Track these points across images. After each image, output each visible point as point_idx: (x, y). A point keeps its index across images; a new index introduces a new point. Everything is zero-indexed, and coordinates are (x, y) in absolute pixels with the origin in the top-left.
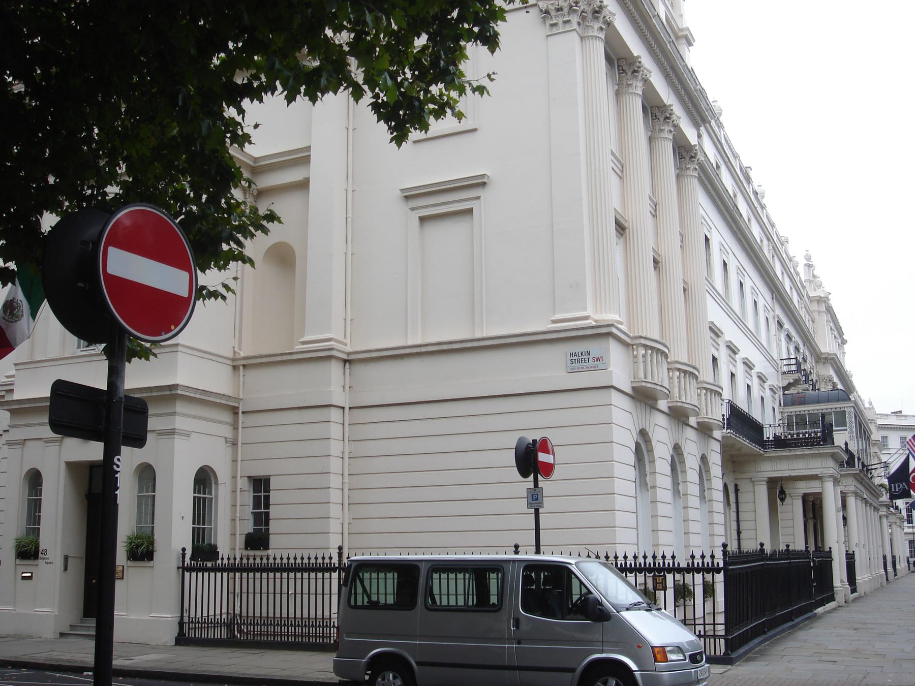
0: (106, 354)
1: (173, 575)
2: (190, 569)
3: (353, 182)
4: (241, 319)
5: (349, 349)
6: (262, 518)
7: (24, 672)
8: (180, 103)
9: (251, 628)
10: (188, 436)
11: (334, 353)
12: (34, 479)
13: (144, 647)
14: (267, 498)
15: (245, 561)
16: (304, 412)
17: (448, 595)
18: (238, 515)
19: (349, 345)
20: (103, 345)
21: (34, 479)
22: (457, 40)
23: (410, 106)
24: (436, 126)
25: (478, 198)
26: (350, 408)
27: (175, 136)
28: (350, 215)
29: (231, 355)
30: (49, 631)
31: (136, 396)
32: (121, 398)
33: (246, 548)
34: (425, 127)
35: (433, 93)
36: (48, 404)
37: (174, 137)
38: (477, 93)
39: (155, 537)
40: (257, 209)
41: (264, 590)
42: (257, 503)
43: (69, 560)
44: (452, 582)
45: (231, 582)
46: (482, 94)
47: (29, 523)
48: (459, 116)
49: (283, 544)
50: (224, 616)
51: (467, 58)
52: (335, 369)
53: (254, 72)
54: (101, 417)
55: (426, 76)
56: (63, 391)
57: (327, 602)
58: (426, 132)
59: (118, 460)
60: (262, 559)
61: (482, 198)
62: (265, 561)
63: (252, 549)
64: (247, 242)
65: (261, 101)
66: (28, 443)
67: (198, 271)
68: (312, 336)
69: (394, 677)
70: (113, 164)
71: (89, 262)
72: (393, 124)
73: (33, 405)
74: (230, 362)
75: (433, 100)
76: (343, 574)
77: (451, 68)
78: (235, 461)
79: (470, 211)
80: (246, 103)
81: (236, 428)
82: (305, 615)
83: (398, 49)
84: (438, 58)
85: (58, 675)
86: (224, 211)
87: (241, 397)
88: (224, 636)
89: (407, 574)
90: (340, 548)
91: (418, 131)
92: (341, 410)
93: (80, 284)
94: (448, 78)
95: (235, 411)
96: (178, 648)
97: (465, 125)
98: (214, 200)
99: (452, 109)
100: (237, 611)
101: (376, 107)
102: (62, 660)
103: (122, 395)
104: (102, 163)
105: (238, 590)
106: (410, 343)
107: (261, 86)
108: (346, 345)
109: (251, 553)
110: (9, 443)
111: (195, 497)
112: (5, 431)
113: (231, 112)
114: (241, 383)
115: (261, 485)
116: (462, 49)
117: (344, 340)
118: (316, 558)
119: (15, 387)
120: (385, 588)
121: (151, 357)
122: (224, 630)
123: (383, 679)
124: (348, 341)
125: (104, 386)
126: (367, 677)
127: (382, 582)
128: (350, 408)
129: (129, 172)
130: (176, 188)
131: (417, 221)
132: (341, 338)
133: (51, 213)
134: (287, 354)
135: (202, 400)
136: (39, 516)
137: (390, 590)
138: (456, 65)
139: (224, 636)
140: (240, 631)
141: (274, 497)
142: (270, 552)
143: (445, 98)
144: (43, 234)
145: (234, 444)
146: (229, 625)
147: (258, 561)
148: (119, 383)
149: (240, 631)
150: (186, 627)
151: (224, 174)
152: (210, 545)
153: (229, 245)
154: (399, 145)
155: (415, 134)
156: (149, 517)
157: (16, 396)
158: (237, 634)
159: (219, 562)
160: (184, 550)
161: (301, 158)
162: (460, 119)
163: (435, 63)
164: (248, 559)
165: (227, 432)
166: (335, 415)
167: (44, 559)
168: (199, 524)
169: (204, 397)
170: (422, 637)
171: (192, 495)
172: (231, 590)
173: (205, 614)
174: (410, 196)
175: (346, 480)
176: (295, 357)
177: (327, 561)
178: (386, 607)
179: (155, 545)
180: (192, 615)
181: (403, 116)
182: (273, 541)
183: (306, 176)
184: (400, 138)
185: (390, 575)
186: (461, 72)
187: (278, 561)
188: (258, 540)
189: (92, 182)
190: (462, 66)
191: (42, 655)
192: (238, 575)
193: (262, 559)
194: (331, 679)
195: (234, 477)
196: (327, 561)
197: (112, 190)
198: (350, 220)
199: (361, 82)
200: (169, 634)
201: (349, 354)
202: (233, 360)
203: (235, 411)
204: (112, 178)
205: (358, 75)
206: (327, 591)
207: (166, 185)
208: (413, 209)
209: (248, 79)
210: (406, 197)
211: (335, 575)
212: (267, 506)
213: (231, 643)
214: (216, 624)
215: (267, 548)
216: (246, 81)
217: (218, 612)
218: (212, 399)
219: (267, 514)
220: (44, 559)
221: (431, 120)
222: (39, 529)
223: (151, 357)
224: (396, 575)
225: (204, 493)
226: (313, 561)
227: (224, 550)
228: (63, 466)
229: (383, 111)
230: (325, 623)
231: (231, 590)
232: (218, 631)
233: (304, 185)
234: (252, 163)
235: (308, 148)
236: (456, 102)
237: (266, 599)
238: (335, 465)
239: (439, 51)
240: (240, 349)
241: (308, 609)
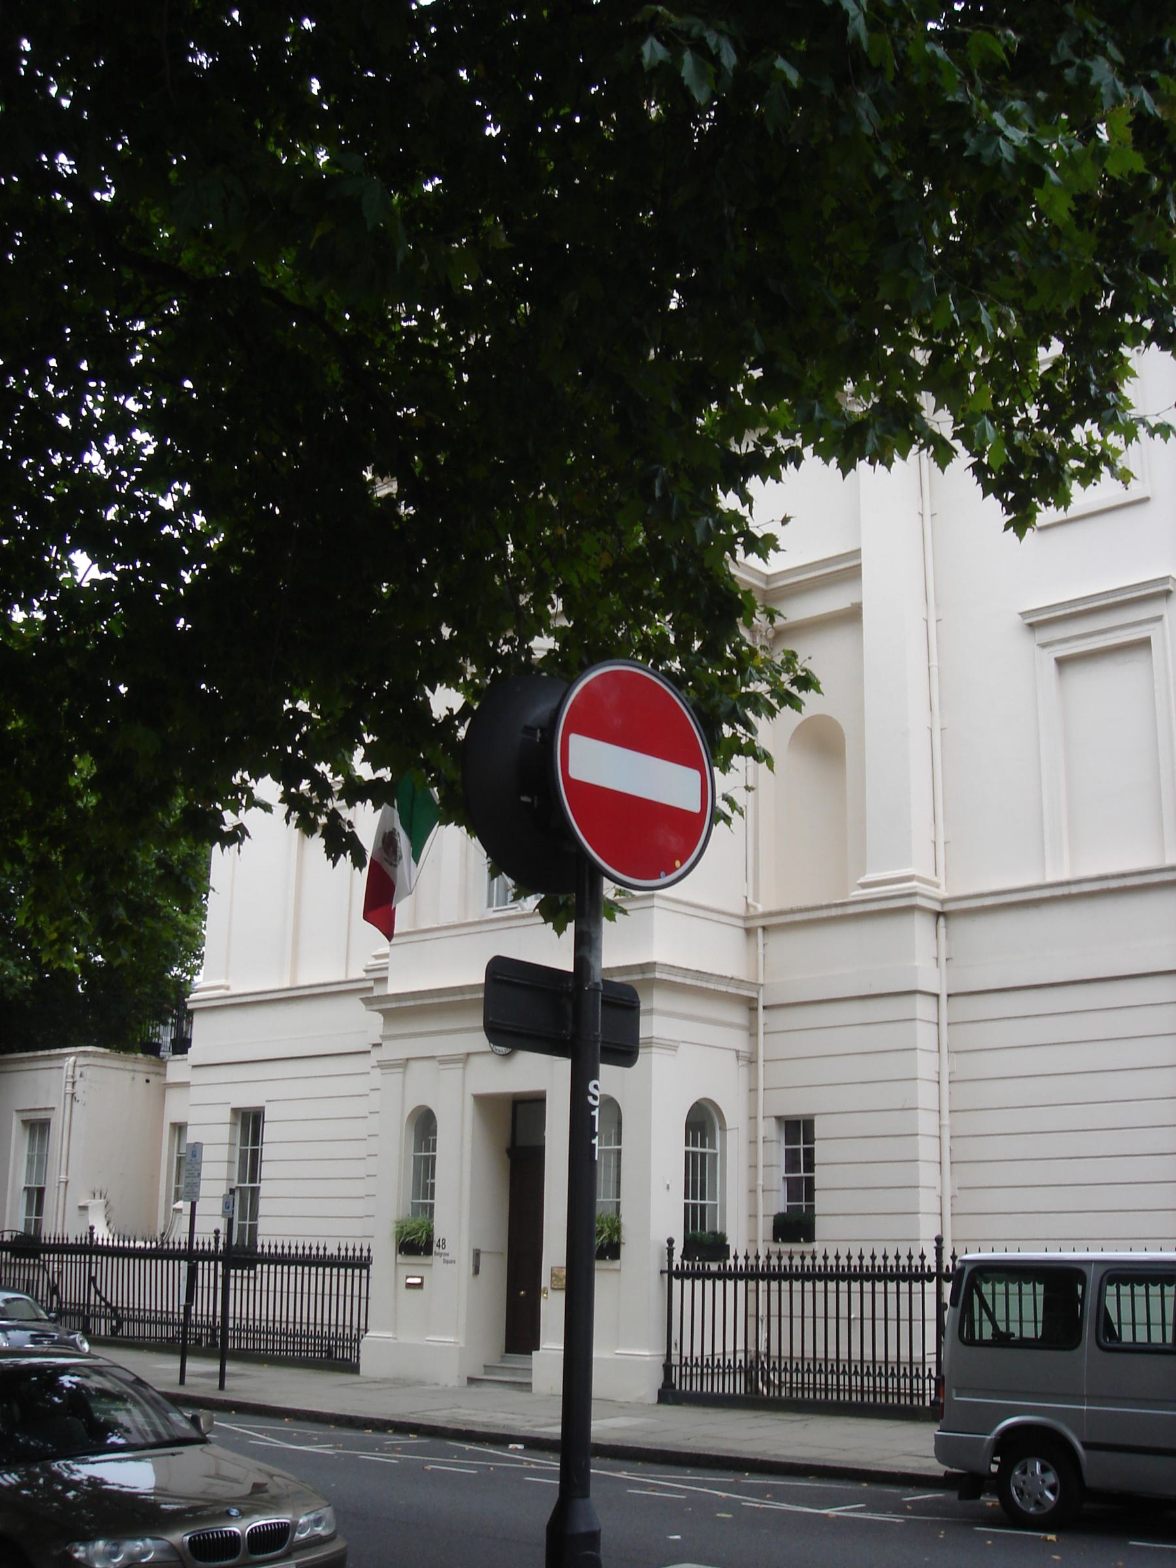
0: (542, 913)
1: (654, 1284)
2: (682, 1275)
3: (937, 605)
4: (756, 849)
5: (943, 893)
6: (801, 1188)
7: (413, 1439)
8: (658, 493)
9: (786, 1377)
10: (674, 1048)
11: (919, 901)
12: (424, 1124)
13: (624, 1408)
14: (809, 1153)
15: (774, 1261)
16: (871, 1004)
17: (1134, 1324)
18: (760, 1182)
19: (943, 887)
20: (543, 896)
21: (424, 1124)
22: (1114, 344)
23: (1040, 464)
24: (1082, 497)
25: (1159, 619)
26: (949, 996)
27: (641, 547)
28: (934, 662)
29: (741, 911)
30: (450, 1374)
31: (617, 979)
32: (597, 984)
33: (775, 1240)
34: (1063, 500)
35: (1077, 439)
36: (482, 995)
37: (639, 550)
38: (1157, 436)
39: (623, 1220)
40: (771, 661)
41: (892, 1313)
42: (792, 1162)
43: (482, 1256)
44: (1140, 1302)
45: (752, 1296)
46: (1166, 437)
47: (416, 1195)
48: (1125, 477)
49: (837, 1235)
50: (740, 1356)
51: (1134, 375)
52: (921, 927)
53: (763, 431)
54: (570, 1014)
55: (1060, 417)
56: (504, 973)
57: (916, 1332)
58: (1065, 510)
59: (596, 1087)
60: (803, 1258)
61: (1166, 619)
62: (808, 1261)
63: (785, 1240)
64: (761, 723)
65: (778, 479)
66: (413, 1064)
67: (716, 770)
68: (881, 871)
69: (1044, 1469)
70: (541, 600)
71: (540, 762)
72: (1011, 495)
73: (419, 1002)
74: (740, 923)
75: (1077, 453)
76: (948, 1287)
77: (1109, 396)
78: (753, 1090)
79: (1145, 643)
80: (754, 484)
81: (753, 1034)
82: (797, 1353)
83: (1008, 373)
84: (1084, 381)
85: (467, 1447)
86: (729, 665)
87: (761, 981)
88: (741, 1389)
89: (1060, 1282)
90: (939, 1240)
91: (1052, 508)
92: (934, 999)
93: (525, 799)
94: (1107, 414)
95: (751, 1005)
96: (662, 1407)
97: (1136, 489)
98: (712, 651)
99: (1111, 465)
100: (763, 1348)
101: (978, 469)
102: (473, 1423)
103: (598, 980)
104: (523, 600)
105: (762, 1312)
106: (1050, 878)
107: (777, 454)
108: (937, 886)
109: (786, 1247)
110: (383, 1065)
111: (687, 1153)
112: (374, 1045)
113: (729, 501)
114: (761, 958)
115: (797, 1130)
116: (1123, 360)
117: (935, 879)
118: (897, 1257)
119: (390, 974)
120: (1023, 1309)
121: (618, 916)
122: (741, 1380)
123: (1024, 1472)
124: (941, 879)
125: (568, 966)
126: (994, 1468)
127: (1014, 1300)
128: (949, 996)
129: (567, 612)
130: (646, 635)
131: (1053, 662)
132: (928, 874)
133: (448, 687)
134: (836, 905)
135: (696, 987)
136: (433, 1185)
137: (1028, 1314)
138: (1116, 390)
139: (741, 1389)
140: (768, 1383)
141: (821, 1151)
142: (817, 1246)
143: (1098, 448)
144: (435, 721)
145: (752, 1061)
146: (751, 1369)
147: (797, 1261)
148: (592, 960)
149: (768, 1383)
150: (675, 1373)
151: (722, 607)
152: (714, 1233)
153: (734, 728)
154: (1020, 534)
155: (1046, 514)
156: (612, 1186)
157: (392, 988)
158: (759, 1387)
159: (730, 1262)
160: (670, 1242)
161: (846, 571)
162: (1125, 483)
163: (1079, 388)
164: (780, 1258)
165: (739, 1040)
166: (923, 1008)
167: (441, 1255)
168: (694, 1198)
169: (699, 983)
170: (1093, 1399)
171: (682, 1148)
172: (752, 1310)
173: (719, 1349)
174: (1037, 623)
175: (946, 1121)
176: (851, 910)
177: (916, 1261)
178: (1024, 1343)
179: (624, 1232)
180: (686, 1352)
181: (1026, 483)
182: (822, 1227)
183: (855, 600)
184: (1021, 519)
185: (1027, 1288)
186: (1125, 399)
187: (832, 1261)
188: (794, 1225)
189: (510, 634)
190: (1128, 389)
191: (439, 1416)
192: (762, 1285)
193: (803, 1258)
194: (929, 1468)
195: (753, 1118)
196: (916, 1261)
197: (542, 645)
198: (934, 670)
199: (948, 434)
200: (649, 1384)
201: (943, 902)
202: (746, 918)
203: (751, 1005)
204: (540, 624)
205: (943, 422)
206: (917, 1314)
207: (629, 629)
208: (1043, 646)
209: (755, 445)
210: (1031, 625)
211: (931, 1287)
212: (810, 1166)
213: (751, 1401)
214: (726, 1369)
215: (810, 1238)
216: (751, 449)
217: (730, 1348)
218: (712, 986)
219: (810, 1182)
220: (441, 1255)
221: (1075, 487)
222: (432, 1206)
223: (618, 916)
224: (1040, 1288)
225: (703, 1145)
226: (891, 1261)
227: (738, 1243)
228: (470, 1103)
229: (993, 480)
230: (913, 1371)
231: (752, 1310)
232: (729, 1380)
233: (852, 616)
234: (762, 585)
235: (857, 553)
236: (1118, 452)
237: (810, 1327)
238: (926, 1095)
239: (1085, 368)
240: (756, 898)
241: (886, 1347)
